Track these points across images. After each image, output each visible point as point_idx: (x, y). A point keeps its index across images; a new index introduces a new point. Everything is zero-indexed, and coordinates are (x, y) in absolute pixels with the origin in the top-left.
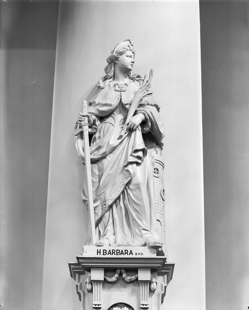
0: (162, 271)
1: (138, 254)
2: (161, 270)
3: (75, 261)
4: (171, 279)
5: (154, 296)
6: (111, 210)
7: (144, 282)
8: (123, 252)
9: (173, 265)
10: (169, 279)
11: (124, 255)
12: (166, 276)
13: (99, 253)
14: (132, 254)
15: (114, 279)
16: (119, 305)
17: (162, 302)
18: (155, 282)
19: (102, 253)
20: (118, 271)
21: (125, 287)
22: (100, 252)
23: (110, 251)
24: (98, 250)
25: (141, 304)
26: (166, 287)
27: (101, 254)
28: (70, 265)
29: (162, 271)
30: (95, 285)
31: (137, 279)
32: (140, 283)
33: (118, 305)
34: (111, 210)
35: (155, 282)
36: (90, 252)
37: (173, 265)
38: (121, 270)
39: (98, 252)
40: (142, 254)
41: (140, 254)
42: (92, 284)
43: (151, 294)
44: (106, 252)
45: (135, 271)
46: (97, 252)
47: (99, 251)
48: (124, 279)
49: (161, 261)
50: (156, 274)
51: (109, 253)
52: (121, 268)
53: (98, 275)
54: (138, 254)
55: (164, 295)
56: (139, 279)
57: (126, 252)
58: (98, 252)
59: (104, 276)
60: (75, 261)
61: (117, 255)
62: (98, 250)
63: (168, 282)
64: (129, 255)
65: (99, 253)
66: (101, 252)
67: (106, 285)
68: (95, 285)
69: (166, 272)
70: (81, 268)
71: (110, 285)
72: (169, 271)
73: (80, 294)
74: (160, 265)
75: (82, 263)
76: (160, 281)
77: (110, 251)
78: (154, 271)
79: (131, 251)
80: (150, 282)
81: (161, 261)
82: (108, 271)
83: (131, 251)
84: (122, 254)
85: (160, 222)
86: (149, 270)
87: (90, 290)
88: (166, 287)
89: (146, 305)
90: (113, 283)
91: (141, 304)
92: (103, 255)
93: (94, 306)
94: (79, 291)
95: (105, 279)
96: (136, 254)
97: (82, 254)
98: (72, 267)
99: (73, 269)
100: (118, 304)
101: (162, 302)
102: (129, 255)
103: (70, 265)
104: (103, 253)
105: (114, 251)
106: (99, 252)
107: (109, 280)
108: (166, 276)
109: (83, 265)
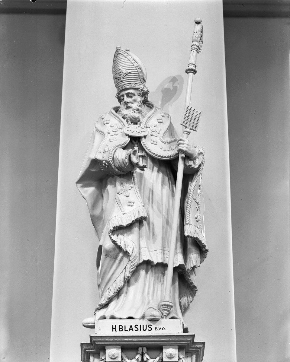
1: (158, 329)
6: (132, 179)
9: (204, 344)
11: (133, 330)
12: (194, 357)
19: (117, 329)
20: (140, 349)
22: (115, 328)
23: (131, 326)
24: (113, 326)
28: (82, 345)
34: (132, 179)
36: (104, 329)
37: (204, 344)
39: (114, 328)
40: (163, 329)
41: (161, 329)
44: (122, 328)
45: (159, 349)
46: (112, 328)
51: (130, 330)
52: (142, 346)
54: (158, 329)
57: (121, 327)
58: (113, 328)
59: (122, 353)
61: (120, 331)
62: (113, 326)
64: (129, 331)
75: (86, 350)
77: (131, 326)
81: (191, 339)
82: (124, 349)
84: (131, 330)
85: (153, 308)
86: (175, 348)
92: (120, 331)
96: (156, 328)
98: (84, 347)
99: (85, 350)
102: (129, 331)
103: (82, 345)
104: (120, 329)
106: (114, 328)
109: (97, 344)
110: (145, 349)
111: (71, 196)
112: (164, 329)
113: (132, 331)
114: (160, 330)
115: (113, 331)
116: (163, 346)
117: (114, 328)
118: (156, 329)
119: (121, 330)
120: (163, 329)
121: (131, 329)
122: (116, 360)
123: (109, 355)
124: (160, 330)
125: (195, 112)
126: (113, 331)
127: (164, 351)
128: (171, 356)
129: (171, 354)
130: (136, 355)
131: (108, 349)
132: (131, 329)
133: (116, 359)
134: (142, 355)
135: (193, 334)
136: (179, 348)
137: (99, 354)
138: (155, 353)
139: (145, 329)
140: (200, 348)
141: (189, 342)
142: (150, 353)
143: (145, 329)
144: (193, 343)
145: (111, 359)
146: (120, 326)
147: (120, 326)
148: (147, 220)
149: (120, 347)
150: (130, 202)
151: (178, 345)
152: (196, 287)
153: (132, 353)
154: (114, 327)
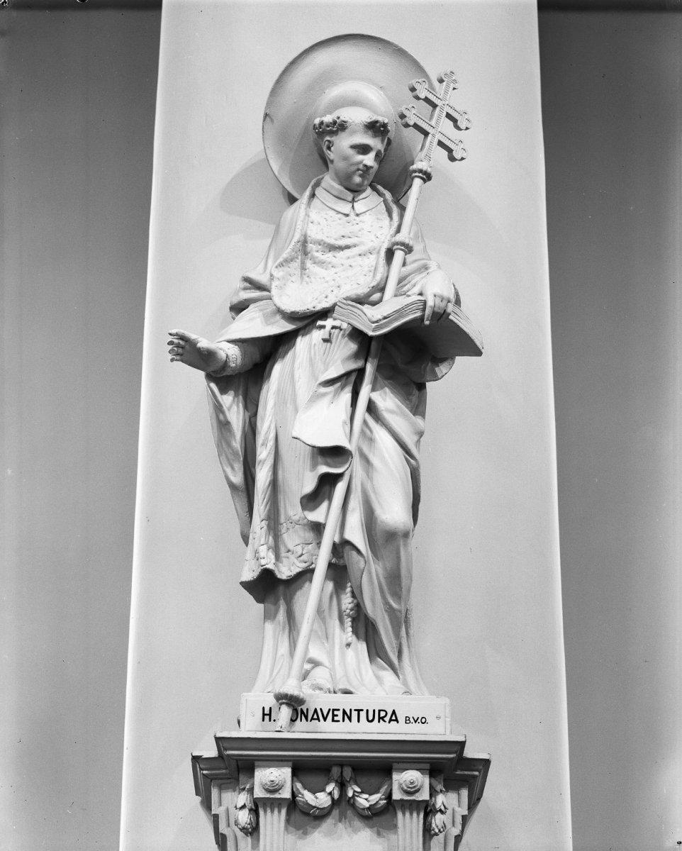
1: (412, 720)
4: (479, 799)
7: (411, 805)
9: (486, 763)
11: (319, 721)
12: (465, 793)
13: (265, 713)
14: (396, 720)
15: (321, 800)
20: (335, 771)
24: (264, 708)
27: (272, 719)
28: (196, 759)
37: (486, 763)
40: (423, 720)
41: (419, 720)
45: (385, 770)
49: (457, 748)
52: (342, 763)
54: (412, 720)
58: (264, 715)
60: (211, 752)
62: (264, 708)
64: (389, 723)
65: (267, 718)
66: (261, 715)
67: (297, 816)
70: (227, 767)
72: (477, 773)
76: (451, 802)
78: (434, 770)
79: (394, 712)
83: (394, 712)
84: (394, 720)
96: (407, 720)
102: (389, 723)
103: (196, 759)
105: (383, 714)
107: (308, 797)
108: (465, 793)
110: (348, 772)
111: (174, 404)
113: (396, 722)
114: (416, 722)
115: (263, 720)
116: (256, 763)
119: (408, 722)
121: (315, 717)
122: (277, 796)
123: (400, 785)
124: (416, 722)
126: (263, 720)
127: (395, 776)
128: (414, 787)
129: (272, 781)
130: (328, 783)
131: (260, 767)
133: (417, 794)
134: (342, 786)
135: (461, 739)
137: (238, 780)
138: (374, 780)
139: (370, 718)
140: (477, 776)
142: (363, 780)
143: (370, 718)
146: (380, 711)
147: (380, 711)
149: (290, 763)
151: (428, 763)
153: (315, 779)
154: (267, 711)
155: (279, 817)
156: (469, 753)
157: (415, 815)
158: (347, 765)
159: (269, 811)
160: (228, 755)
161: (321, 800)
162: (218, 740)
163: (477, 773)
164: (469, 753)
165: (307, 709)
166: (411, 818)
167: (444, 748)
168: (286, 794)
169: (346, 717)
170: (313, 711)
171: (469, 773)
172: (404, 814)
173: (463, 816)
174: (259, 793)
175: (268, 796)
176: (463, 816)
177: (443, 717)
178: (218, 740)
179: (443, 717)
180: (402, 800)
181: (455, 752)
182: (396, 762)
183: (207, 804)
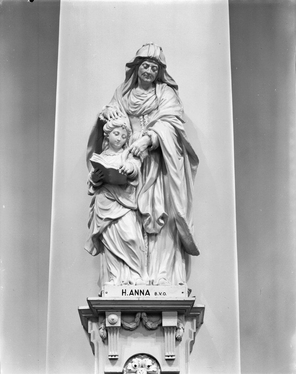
0: (191, 313)
2: (190, 312)
3: (87, 307)
4: (202, 323)
5: (182, 344)
7: (117, 328)
8: (132, 292)
10: (199, 324)
11: (133, 295)
12: (195, 321)
13: (123, 292)
14: (149, 294)
16: (139, 356)
17: (191, 352)
18: (182, 327)
20: (139, 315)
21: (145, 335)
23: (132, 291)
24: (123, 290)
25: (166, 356)
26: (195, 333)
27: (126, 295)
28: (80, 311)
29: (191, 313)
30: (110, 335)
31: (161, 324)
32: (165, 329)
33: (139, 356)
35: (182, 327)
36: (113, 292)
38: (144, 315)
40: (164, 294)
41: (162, 294)
42: (107, 331)
43: (177, 342)
47: (124, 291)
48: (145, 327)
50: (183, 318)
52: (142, 311)
53: (114, 318)
54: (158, 293)
55: (192, 343)
56: (164, 325)
58: (123, 293)
60: (87, 307)
62: (123, 290)
63: (197, 328)
64: (130, 295)
68: (110, 335)
69: (195, 315)
70: (95, 313)
71: (128, 332)
72: (199, 313)
73: (94, 346)
74: (190, 306)
76: (187, 327)
77: (132, 291)
79: (148, 291)
80: (176, 328)
81: (191, 303)
83: (148, 291)
86: (173, 316)
87: (105, 337)
88: (195, 333)
89: (172, 356)
90: (130, 329)
91: (166, 356)
93: (110, 357)
94: (92, 340)
95: (122, 325)
96: (156, 294)
97: (101, 296)
100: (139, 355)
101: (191, 352)
102: (130, 295)
103: (80, 311)
107: (127, 325)
112: (165, 294)
114: (160, 295)
115: (123, 295)
117: (124, 293)
118: (155, 294)
120: (164, 294)
121: (132, 293)
122: (115, 325)
125: (201, 100)
126: (123, 295)
132: (132, 293)
135: (203, 306)
136: (178, 314)
140: (199, 314)
141: (190, 306)
144: (192, 307)
145: (110, 324)
148: (165, 219)
150: (117, 113)
152: (198, 161)
153: (130, 319)
155: (173, 335)
156: (196, 305)
157: (115, 334)
158: (144, 312)
159: (112, 334)
160: (94, 308)
161: (132, 326)
162: (89, 301)
163: (199, 313)
164: (196, 305)
165: (143, 290)
166: (113, 335)
167: (152, 303)
168: (119, 324)
169: (137, 292)
170: (134, 292)
171: (195, 313)
172: (167, 333)
173: (194, 333)
174: (108, 325)
175: (111, 326)
176: (194, 333)
177: (105, 293)
178: (89, 301)
179: (105, 293)
180: (109, 327)
181: (190, 305)
182: (164, 311)
183: (86, 329)
